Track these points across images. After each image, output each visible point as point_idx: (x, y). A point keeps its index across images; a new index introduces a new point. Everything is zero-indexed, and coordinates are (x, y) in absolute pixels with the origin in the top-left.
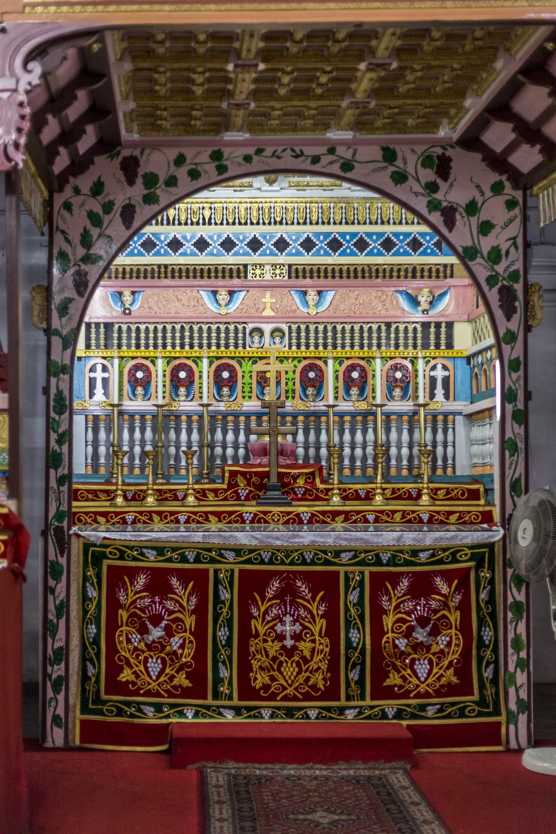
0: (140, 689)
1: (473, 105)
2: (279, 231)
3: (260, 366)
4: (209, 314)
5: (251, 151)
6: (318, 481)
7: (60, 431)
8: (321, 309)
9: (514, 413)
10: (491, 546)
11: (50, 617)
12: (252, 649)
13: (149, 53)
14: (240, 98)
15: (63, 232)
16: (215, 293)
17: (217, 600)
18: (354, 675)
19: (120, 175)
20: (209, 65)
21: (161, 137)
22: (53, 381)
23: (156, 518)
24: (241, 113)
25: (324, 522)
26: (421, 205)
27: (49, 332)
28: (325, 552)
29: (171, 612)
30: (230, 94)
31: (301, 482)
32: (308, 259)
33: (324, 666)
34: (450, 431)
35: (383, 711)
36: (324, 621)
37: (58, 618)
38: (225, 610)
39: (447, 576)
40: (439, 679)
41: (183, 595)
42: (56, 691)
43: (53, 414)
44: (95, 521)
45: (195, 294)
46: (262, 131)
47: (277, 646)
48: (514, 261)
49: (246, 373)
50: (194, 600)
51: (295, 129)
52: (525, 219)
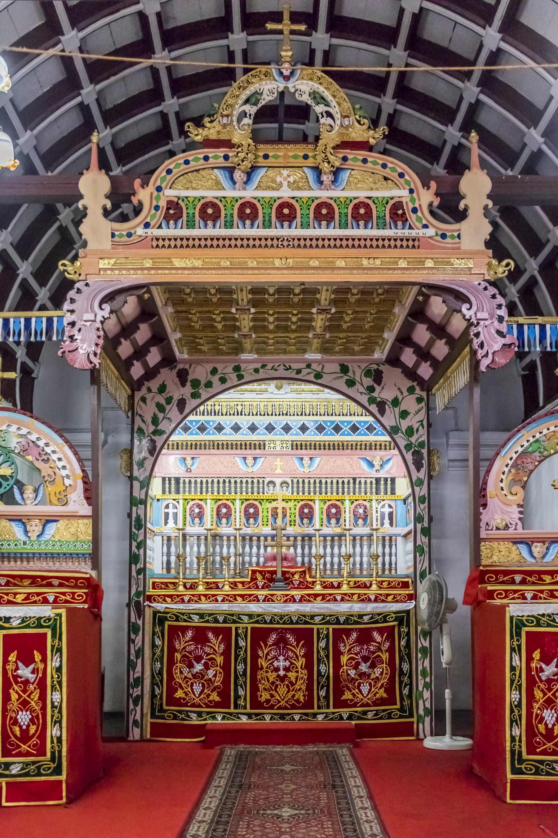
0: (188, 702)
1: (390, 336)
2: (284, 420)
3: (274, 504)
4: (241, 472)
5: (258, 366)
6: (307, 576)
7: (139, 540)
8: (311, 469)
9: (422, 529)
10: (408, 612)
11: (132, 658)
12: (259, 677)
13: (183, 302)
14: (245, 331)
15: (140, 416)
16: (245, 458)
18: (323, 693)
19: (177, 380)
20: (221, 309)
21: (202, 357)
22: (134, 509)
23: (203, 598)
24: (248, 340)
25: (309, 601)
26: (364, 399)
27: (131, 478)
28: (305, 616)
29: (208, 654)
30: (238, 329)
31: (297, 577)
33: (304, 688)
34: (394, 546)
35: (340, 715)
36: (304, 659)
37: (137, 659)
38: (242, 653)
39: (381, 631)
40: (375, 695)
41: (216, 644)
42: (136, 704)
43: (134, 530)
44: (165, 600)
45: (232, 459)
46: (266, 354)
47: (275, 675)
48: (421, 436)
49: (265, 508)
50: (222, 646)
51: (285, 352)
52: (428, 409)
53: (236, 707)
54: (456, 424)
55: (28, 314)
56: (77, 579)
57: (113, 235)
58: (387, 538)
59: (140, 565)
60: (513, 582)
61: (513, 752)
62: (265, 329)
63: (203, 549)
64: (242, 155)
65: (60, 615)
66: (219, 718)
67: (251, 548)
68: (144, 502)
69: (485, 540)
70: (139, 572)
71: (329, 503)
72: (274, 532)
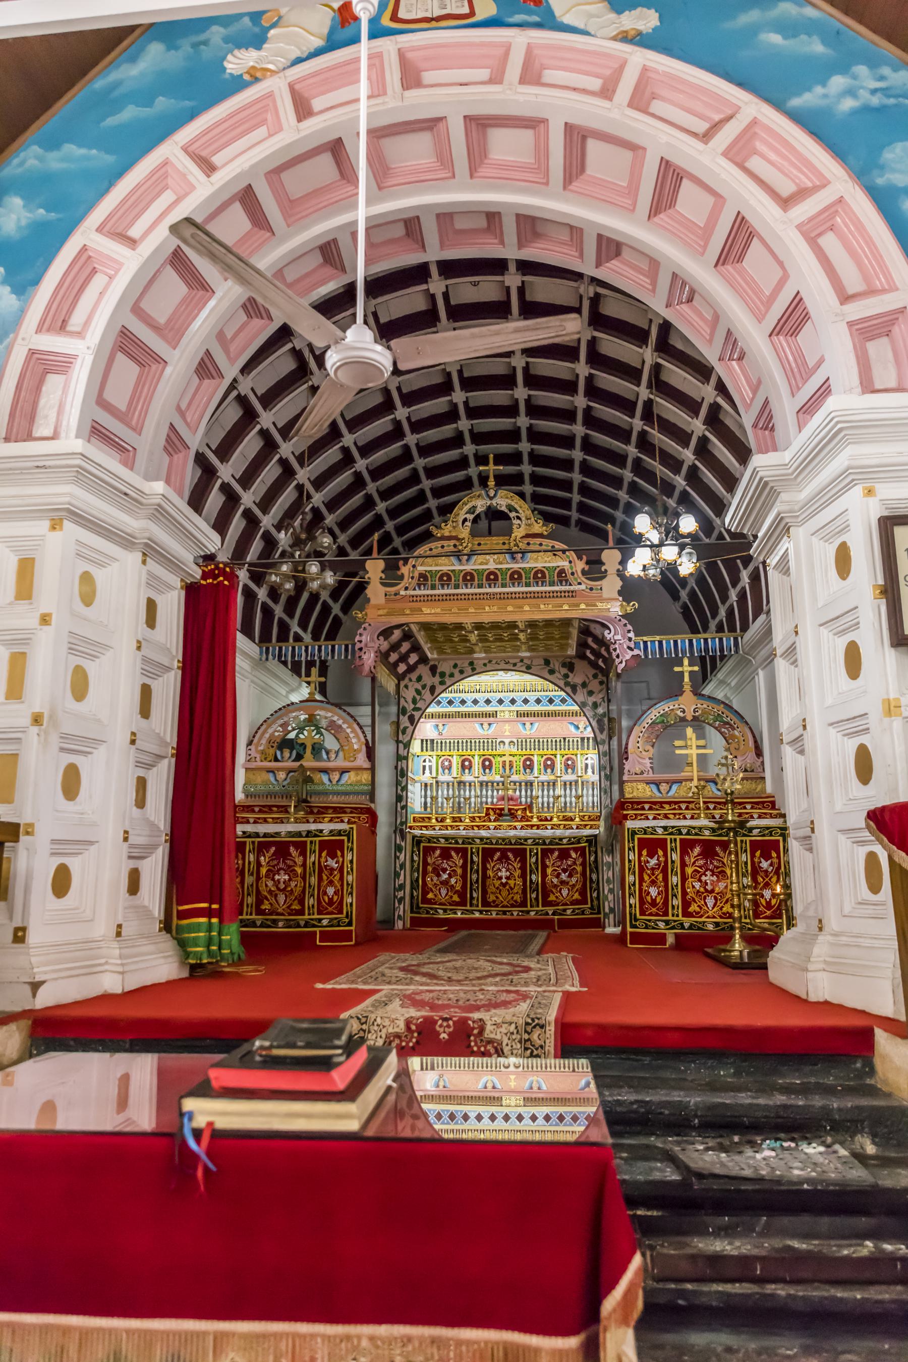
3: (504, 758)
5: (486, 661)
16: (482, 724)
17: (472, 862)
18: (534, 896)
26: (562, 685)
27: (398, 742)
29: (451, 867)
31: (519, 812)
32: (526, 708)
41: (457, 860)
42: (400, 903)
47: (499, 882)
49: (497, 762)
50: (461, 861)
53: (471, 906)
54: (649, 694)
55: (333, 643)
56: (361, 808)
57: (386, 595)
58: (568, 783)
59: (403, 803)
60: (643, 809)
61: (631, 914)
62: (487, 641)
63: (451, 792)
64: (464, 545)
65: (352, 828)
66: (459, 914)
67: (487, 791)
68: (406, 758)
69: (627, 781)
70: (402, 808)
71: (545, 757)
72: (502, 779)
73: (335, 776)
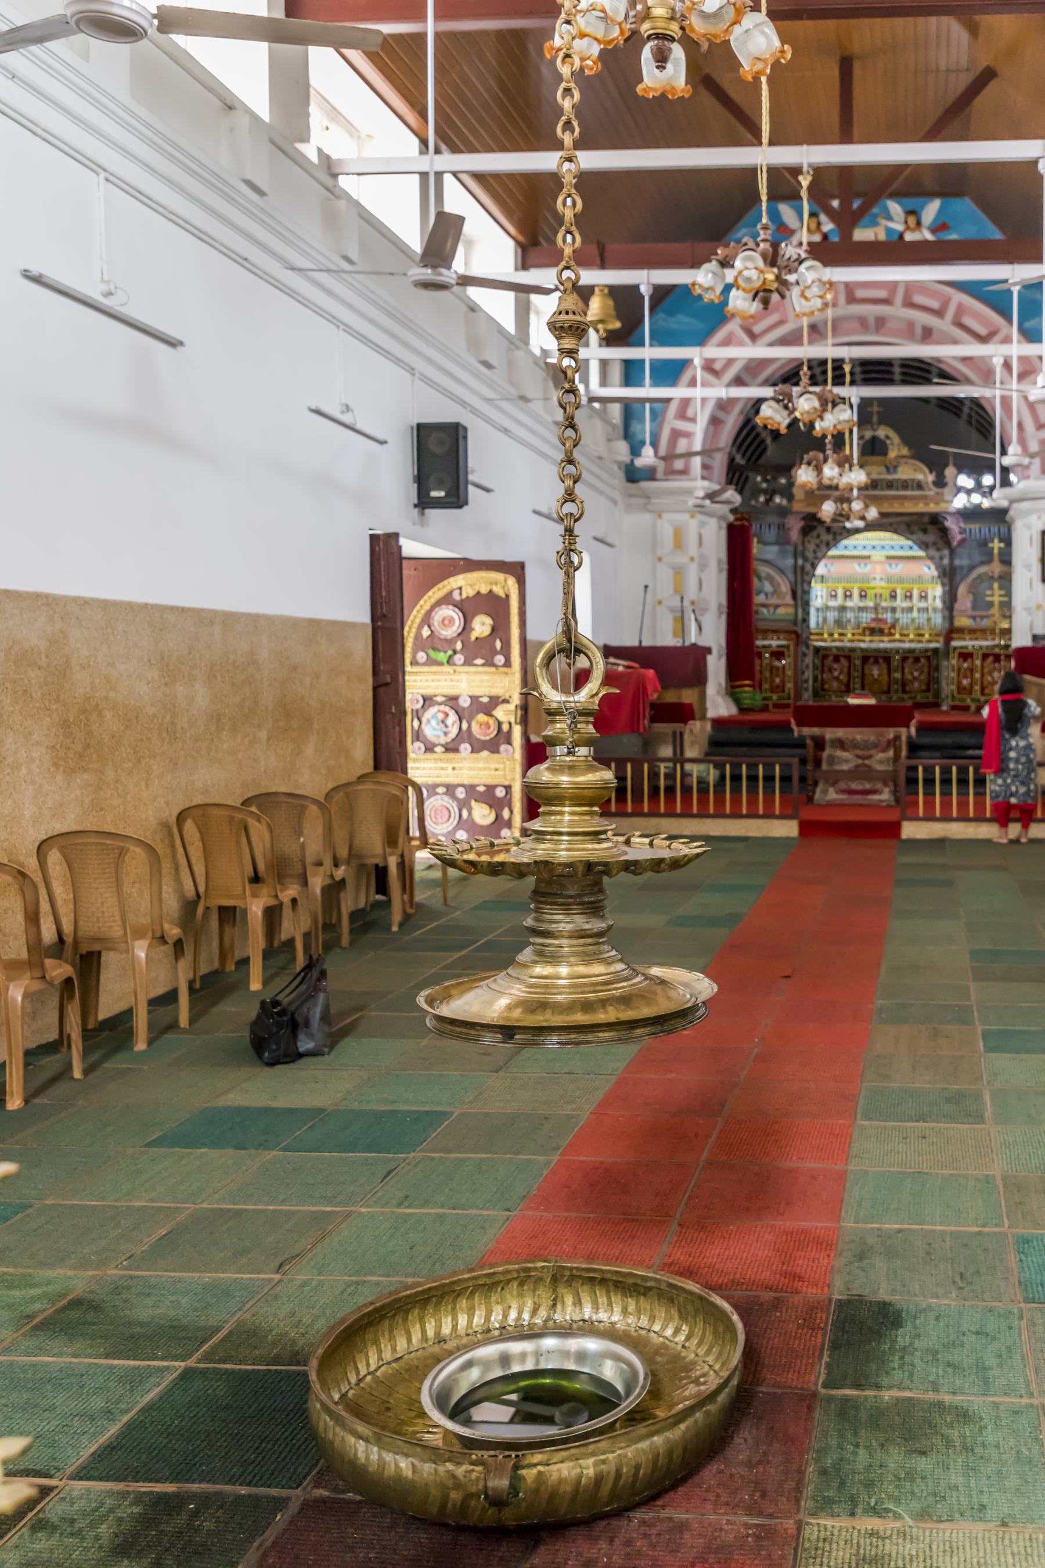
73: (772, 609)
